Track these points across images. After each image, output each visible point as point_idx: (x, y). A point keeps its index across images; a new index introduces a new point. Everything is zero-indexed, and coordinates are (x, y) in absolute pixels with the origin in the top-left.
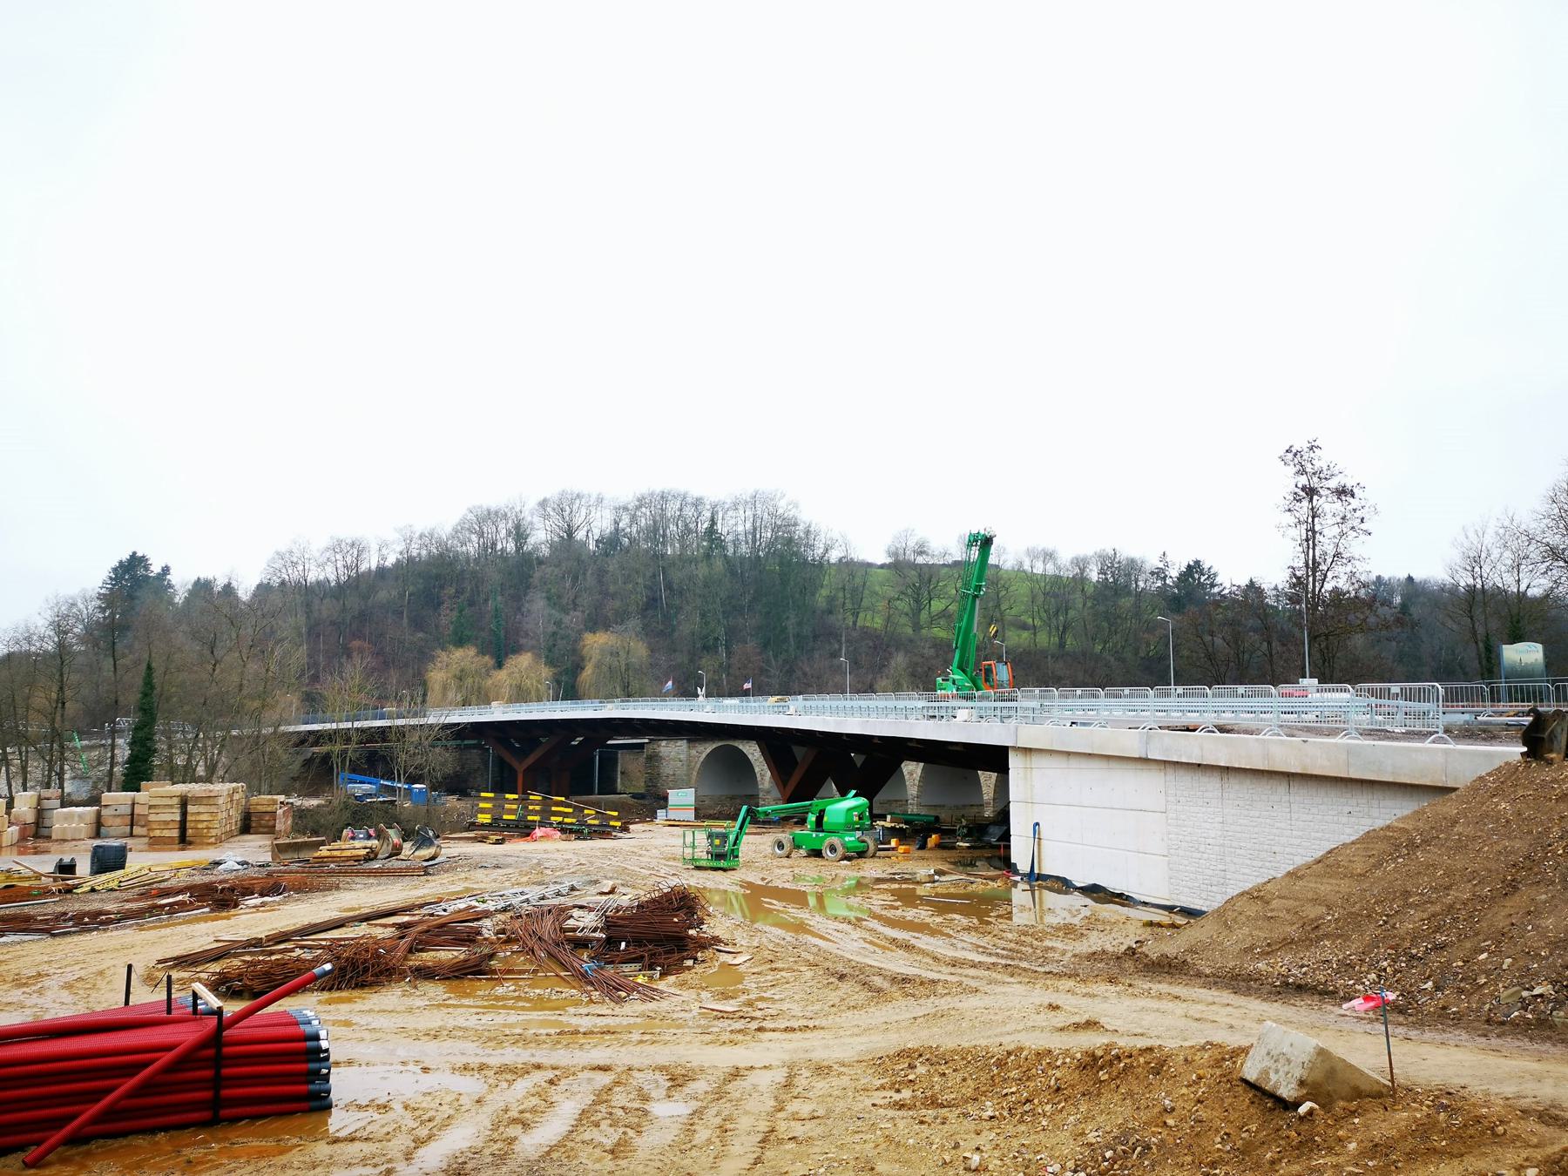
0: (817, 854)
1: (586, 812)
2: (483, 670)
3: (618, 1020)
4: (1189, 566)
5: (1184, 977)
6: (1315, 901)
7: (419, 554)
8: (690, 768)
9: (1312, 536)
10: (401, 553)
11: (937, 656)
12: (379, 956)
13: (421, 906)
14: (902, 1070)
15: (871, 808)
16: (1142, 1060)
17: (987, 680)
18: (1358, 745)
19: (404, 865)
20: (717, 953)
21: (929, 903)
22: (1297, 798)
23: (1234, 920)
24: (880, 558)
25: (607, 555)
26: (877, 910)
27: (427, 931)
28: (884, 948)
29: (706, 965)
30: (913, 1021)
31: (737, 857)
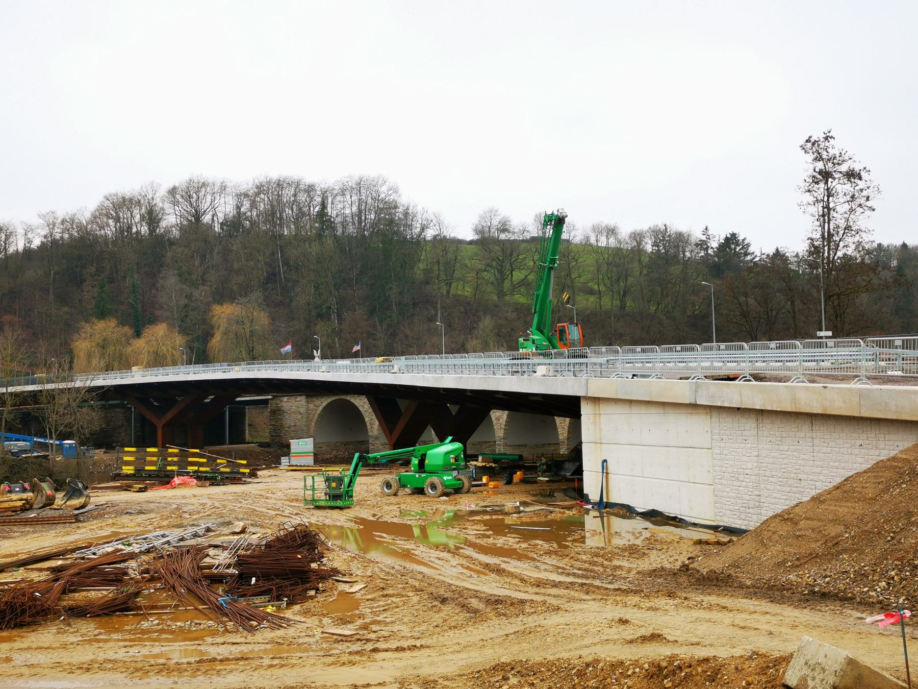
0: (420, 491)
1: (219, 461)
2: (124, 339)
3: (250, 647)
4: (727, 238)
5: (730, 589)
6: (836, 521)
7: (62, 238)
8: (309, 420)
9: (826, 214)
10: (45, 237)
11: (519, 318)
12: (35, 599)
13: (73, 551)
14: (497, 682)
15: (465, 451)
16: (700, 669)
17: (561, 339)
18: (868, 390)
19: (57, 513)
20: (336, 583)
21: (516, 531)
22: (818, 434)
23: (769, 538)
24: (468, 235)
25: (231, 236)
26: (472, 539)
27: (79, 574)
28: (478, 572)
29: (327, 594)
30: (505, 638)
31: (351, 497)
